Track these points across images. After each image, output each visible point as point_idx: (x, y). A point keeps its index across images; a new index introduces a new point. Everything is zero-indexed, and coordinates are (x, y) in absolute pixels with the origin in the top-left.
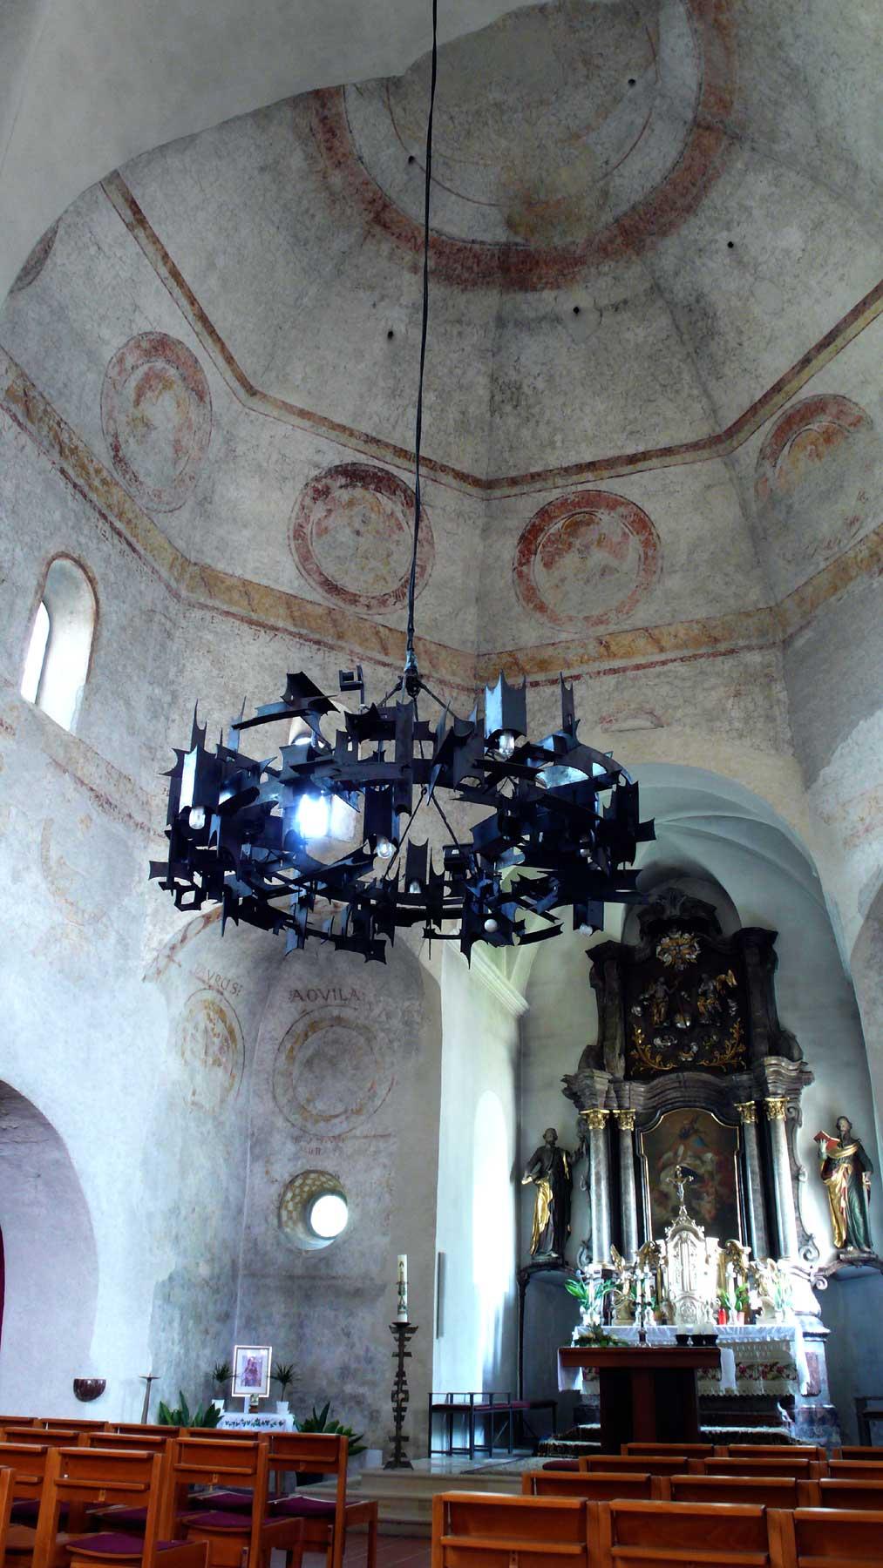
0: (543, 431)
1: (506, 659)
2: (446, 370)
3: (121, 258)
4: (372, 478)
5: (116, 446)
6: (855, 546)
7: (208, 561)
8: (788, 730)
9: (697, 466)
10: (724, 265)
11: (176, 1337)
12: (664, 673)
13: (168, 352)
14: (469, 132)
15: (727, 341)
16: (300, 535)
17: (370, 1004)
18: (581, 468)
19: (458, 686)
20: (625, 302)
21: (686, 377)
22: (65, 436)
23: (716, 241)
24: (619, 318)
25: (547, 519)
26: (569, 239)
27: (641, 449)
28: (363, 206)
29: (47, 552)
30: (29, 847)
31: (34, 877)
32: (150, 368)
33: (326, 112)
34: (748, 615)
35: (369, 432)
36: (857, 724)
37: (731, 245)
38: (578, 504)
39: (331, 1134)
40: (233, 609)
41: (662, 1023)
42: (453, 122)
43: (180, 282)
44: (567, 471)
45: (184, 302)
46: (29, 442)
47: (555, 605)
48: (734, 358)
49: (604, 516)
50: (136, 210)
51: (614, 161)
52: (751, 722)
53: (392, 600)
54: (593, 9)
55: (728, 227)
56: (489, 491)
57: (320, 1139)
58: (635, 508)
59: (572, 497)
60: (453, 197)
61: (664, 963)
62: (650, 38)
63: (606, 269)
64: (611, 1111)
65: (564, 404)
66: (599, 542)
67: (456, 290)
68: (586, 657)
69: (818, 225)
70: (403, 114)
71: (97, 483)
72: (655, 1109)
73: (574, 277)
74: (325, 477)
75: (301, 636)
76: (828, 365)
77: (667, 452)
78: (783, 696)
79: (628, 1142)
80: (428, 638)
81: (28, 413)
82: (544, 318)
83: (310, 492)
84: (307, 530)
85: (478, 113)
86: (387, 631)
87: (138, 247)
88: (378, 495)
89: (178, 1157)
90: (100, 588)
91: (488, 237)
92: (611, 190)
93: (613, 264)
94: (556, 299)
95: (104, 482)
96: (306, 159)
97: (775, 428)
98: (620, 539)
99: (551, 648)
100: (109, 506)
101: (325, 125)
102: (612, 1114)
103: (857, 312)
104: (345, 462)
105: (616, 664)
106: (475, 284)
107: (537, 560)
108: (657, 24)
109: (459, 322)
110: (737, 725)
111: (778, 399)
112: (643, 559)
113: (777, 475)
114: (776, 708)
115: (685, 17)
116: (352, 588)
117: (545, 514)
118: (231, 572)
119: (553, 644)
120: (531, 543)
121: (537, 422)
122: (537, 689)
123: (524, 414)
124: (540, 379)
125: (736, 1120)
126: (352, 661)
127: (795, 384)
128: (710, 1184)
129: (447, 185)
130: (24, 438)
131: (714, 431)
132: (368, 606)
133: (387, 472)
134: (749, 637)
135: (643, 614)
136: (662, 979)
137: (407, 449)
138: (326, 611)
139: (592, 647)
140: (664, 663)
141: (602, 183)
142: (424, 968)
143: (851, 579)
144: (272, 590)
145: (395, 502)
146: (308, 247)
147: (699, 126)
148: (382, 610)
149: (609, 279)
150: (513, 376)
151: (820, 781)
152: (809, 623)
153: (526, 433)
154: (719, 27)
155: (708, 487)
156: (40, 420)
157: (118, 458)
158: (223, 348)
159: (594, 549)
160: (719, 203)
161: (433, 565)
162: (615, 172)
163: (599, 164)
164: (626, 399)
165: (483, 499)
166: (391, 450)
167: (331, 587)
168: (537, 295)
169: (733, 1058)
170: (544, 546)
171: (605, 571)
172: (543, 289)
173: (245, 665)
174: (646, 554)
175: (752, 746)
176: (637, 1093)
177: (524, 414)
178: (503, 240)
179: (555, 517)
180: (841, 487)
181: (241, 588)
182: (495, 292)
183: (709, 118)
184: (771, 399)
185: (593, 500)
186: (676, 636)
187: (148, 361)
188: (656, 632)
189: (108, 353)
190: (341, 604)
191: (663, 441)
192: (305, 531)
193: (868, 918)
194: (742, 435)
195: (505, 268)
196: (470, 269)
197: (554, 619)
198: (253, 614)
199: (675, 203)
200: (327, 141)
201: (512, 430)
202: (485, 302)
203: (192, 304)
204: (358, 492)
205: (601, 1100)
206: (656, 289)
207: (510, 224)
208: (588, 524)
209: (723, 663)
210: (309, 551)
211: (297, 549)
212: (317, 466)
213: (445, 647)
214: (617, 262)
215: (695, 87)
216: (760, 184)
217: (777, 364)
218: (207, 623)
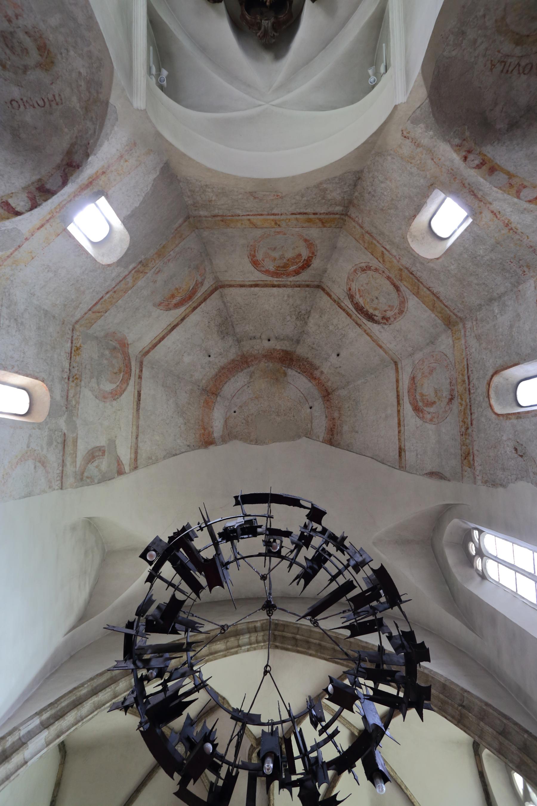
0: (291, 301)
3: (413, 445)
8: (182, 186)
9: (230, 279)
10: (213, 349)
12: (248, 211)
14: (290, 410)
15: (214, 323)
17: (484, 56)
18: (279, 286)
19: (354, 221)
20: (251, 339)
21: (232, 310)
23: (215, 357)
24: (254, 334)
26: (266, 364)
27: (252, 289)
28: (331, 401)
33: (331, 437)
35: (358, 328)
37: (210, 356)
38: (282, 274)
43: (399, 420)
44: (285, 286)
45: (401, 414)
49: (272, 268)
50: (400, 453)
53: (372, 268)
54: (241, 439)
55: (210, 362)
56: (319, 284)
59: (284, 277)
60: (301, 390)
65: (281, 309)
67: (310, 359)
69: (178, 363)
70: (308, 424)
77: (242, 286)
80: (362, 247)
82: (282, 340)
83: (390, 322)
85: (285, 415)
86: (379, 259)
88: (363, 305)
91: (294, 373)
92: (249, 377)
93: (253, 353)
96: (343, 427)
97: (196, 294)
98: (266, 259)
99: (304, 226)
101: (333, 433)
103: (163, 338)
104: (372, 323)
105: (272, 217)
106: (303, 359)
108: (223, 431)
109: (312, 348)
110: (209, 190)
111: (195, 305)
112: (256, 251)
113: (195, 278)
116: (388, 282)
117: (297, 273)
118: (436, 317)
119: (303, 227)
121: (293, 305)
123: (297, 309)
126: (400, 259)
127: (187, 311)
129: (302, 395)
132: (384, 272)
133: (357, 311)
139: (283, 224)
141: (252, 380)
142: (427, 88)
143: (156, 254)
145: (358, 300)
146: (354, 398)
147: (216, 394)
149: (255, 347)
150: (298, 323)
151: (158, 169)
153: (298, 302)
154: (205, 429)
155: (226, 271)
158: (397, 387)
165: (323, 282)
166: (352, 318)
167: (397, 288)
168: (282, 348)
170: (300, 262)
172: (280, 350)
178: (289, 370)
179: (293, 271)
182: (297, 353)
183: (212, 397)
185: (275, 274)
188: (251, 226)
190: (394, 279)
193: (107, 103)
194: (211, 289)
195: (291, 360)
196: (303, 365)
202: (301, 351)
204: (371, 311)
206: (239, 341)
207: (285, 374)
208: (279, 266)
210: (400, 304)
211: (405, 307)
215: (215, 408)
216: (197, 376)
217: (194, 317)
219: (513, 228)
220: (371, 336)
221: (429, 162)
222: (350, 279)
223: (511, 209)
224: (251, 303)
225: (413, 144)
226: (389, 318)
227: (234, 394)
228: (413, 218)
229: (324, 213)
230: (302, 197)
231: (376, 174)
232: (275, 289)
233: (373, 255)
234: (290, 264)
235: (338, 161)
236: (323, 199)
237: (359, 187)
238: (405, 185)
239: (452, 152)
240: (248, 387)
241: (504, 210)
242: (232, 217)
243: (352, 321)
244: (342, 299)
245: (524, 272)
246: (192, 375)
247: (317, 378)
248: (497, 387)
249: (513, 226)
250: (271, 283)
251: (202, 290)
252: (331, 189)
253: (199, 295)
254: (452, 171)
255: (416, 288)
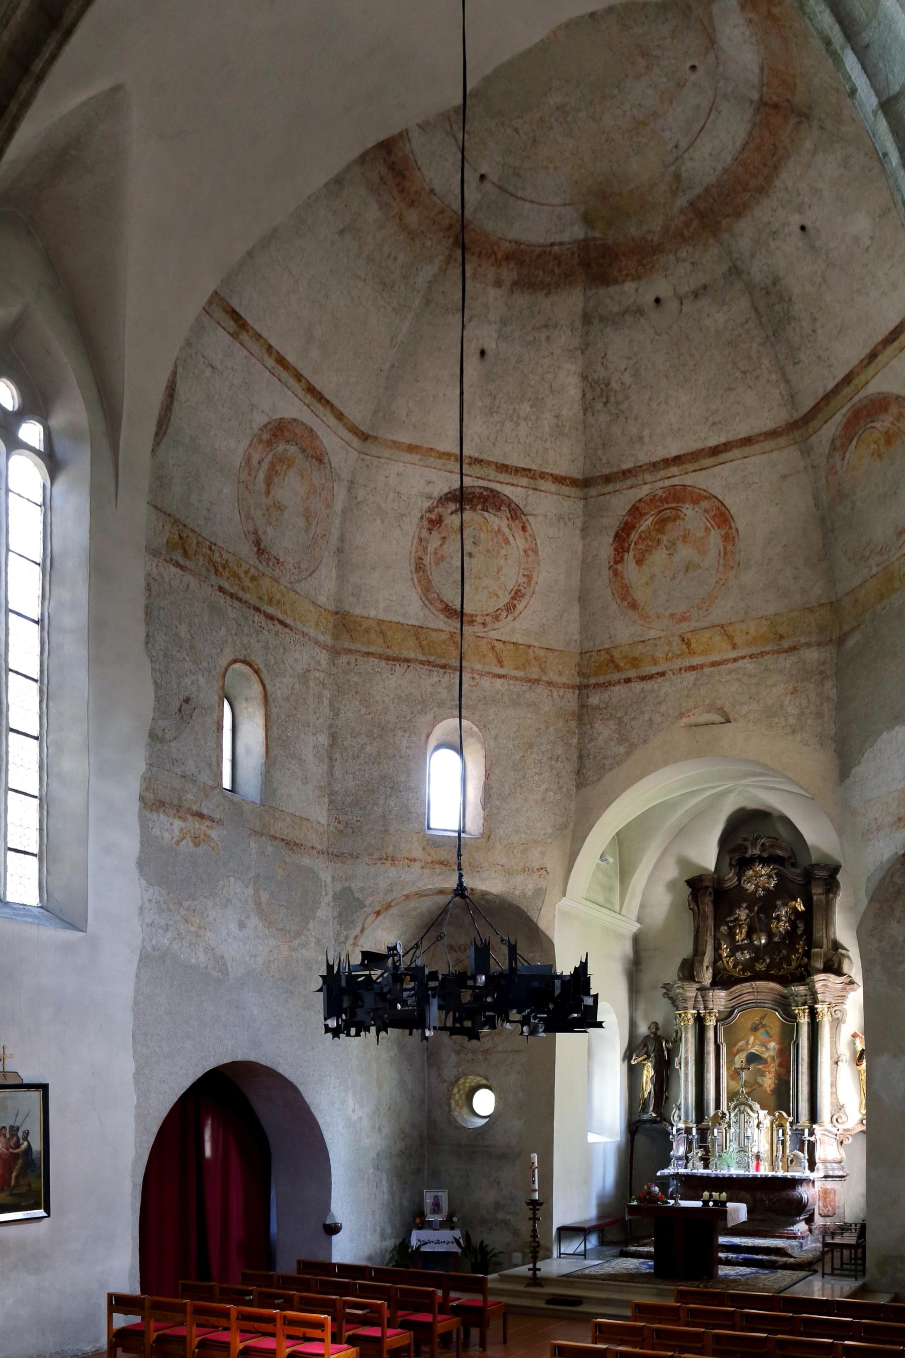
0: (633, 429)
1: (604, 656)
2: (537, 378)
4: (479, 498)
5: (257, 541)
6: (900, 557)
7: (347, 608)
8: (833, 726)
9: (775, 454)
11: (385, 1190)
13: (286, 433)
14: (535, 140)
15: (802, 327)
16: (420, 568)
18: (668, 462)
20: (705, 287)
21: (765, 362)
22: (216, 558)
23: (789, 224)
25: (638, 516)
26: (645, 228)
27: (723, 440)
28: (442, 234)
29: (221, 667)
30: (246, 901)
31: (254, 921)
32: (273, 456)
34: (811, 610)
36: (882, 733)
37: (803, 228)
39: (482, 1049)
40: (372, 649)
41: (742, 940)
42: (518, 133)
44: (654, 466)
45: (292, 382)
46: (191, 578)
47: (645, 602)
48: (809, 345)
51: (683, 145)
52: (803, 719)
53: (505, 613)
55: (800, 209)
56: (586, 490)
57: (474, 1052)
58: (717, 503)
60: (528, 205)
61: (748, 890)
62: (705, 28)
63: (685, 254)
64: (698, 1011)
65: (650, 399)
66: (685, 538)
68: (670, 654)
71: (247, 582)
72: (733, 1009)
73: (653, 267)
74: (437, 507)
75: (429, 663)
76: (892, 363)
77: (747, 441)
78: (833, 693)
79: (711, 1034)
80: (536, 644)
81: (185, 554)
82: (626, 311)
83: (425, 523)
84: (426, 561)
86: (501, 644)
87: (244, 350)
88: (486, 514)
89: (375, 1077)
90: (265, 674)
91: (566, 237)
92: (683, 174)
93: (690, 249)
94: (637, 290)
95: (253, 579)
96: (381, 208)
97: (845, 420)
98: (703, 534)
99: (641, 646)
100: (261, 598)
102: (699, 1014)
105: (696, 660)
106: (558, 286)
107: (629, 557)
108: (711, 17)
109: (546, 326)
111: (848, 390)
112: (722, 554)
114: (825, 704)
115: (738, 9)
117: (636, 512)
119: (643, 642)
120: (624, 541)
121: (626, 418)
122: (629, 685)
124: (627, 374)
125: (793, 1018)
126: (473, 678)
127: (863, 378)
128: (772, 1065)
129: (520, 194)
130: (188, 578)
131: (792, 417)
132: (484, 624)
133: (492, 490)
134: (810, 633)
135: (721, 611)
136: (745, 905)
137: (508, 463)
138: (449, 636)
140: (735, 660)
141: (673, 168)
144: (403, 625)
146: (396, 288)
148: (497, 625)
149: (687, 265)
150: (601, 373)
152: (859, 625)
156: (196, 553)
157: (261, 551)
159: (680, 545)
160: (790, 183)
161: (539, 572)
162: (686, 155)
163: (669, 148)
164: (708, 389)
165: (581, 499)
169: (797, 968)
170: (635, 543)
171: (689, 567)
172: (624, 281)
173: (386, 699)
174: (725, 548)
175: (801, 742)
176: (720, 999)
177: (614, 411)
178: (581, 236)
179: (645, 514)
180: (895, 493)
181: (376, 629)
184: (842, 390)
186: (747, 633)
187: (271, 450)
189: (237, 460)
191: (743, 430)
192: (424, 562)
193: (871, 901)
194: (815, 423)
197: (645, 617)
198: (388, 650)
199: (747, 184)
200: (398, 185)
201: (603, 426)
203: (300, 380)
205: (691, 1003)
206: (735, 271)
207: (587, 220)
208: (674, 520)
209: (785, 659)
211: (419, 582)
212: (430, 497)
213: (551, 650)
214: (694, 246)
215: (757, 71)
218: (352, 666)
219: (385, 861)
220: (440, 458)
221: (504, 861)
222: (532, 550)
223: (402, 879)
224: (722, 396)
225: (530, 867)
226: (430, 530)
227: (712, 117)
228: (488, 773)
229: (614, 685)
230: (650, 720)
231: (558, 797)
232: (674, 451)
233: (514, 643)
234: (653, 534)
235: (613, 801)
236: (620, 719)
237: (575, 757)
238: (517, 810)
239: (488, 890)
240: (676, 147)
241: (406, 873)
242: (763, 650)
243: (491, 459)
244: (530, 492)
245: (339, 823)
246: (845, 167)
247: (504, 263)
248: (248, 679)
249: (388, 863)
250: (685, 466)
251: (833, 430)
252: (612, 743)
253: (838, 417)
254: (478, 870)
255: (424, 643)
